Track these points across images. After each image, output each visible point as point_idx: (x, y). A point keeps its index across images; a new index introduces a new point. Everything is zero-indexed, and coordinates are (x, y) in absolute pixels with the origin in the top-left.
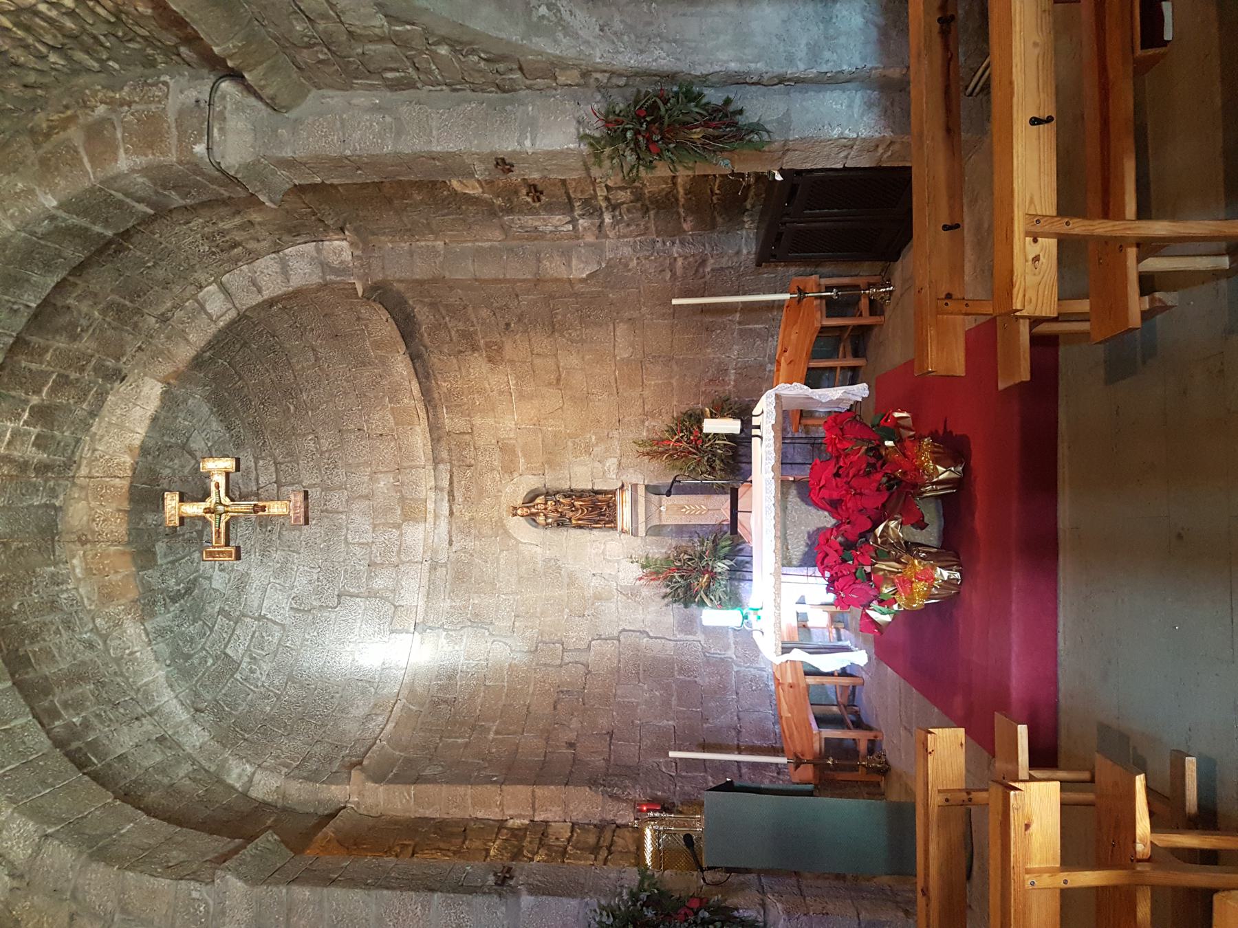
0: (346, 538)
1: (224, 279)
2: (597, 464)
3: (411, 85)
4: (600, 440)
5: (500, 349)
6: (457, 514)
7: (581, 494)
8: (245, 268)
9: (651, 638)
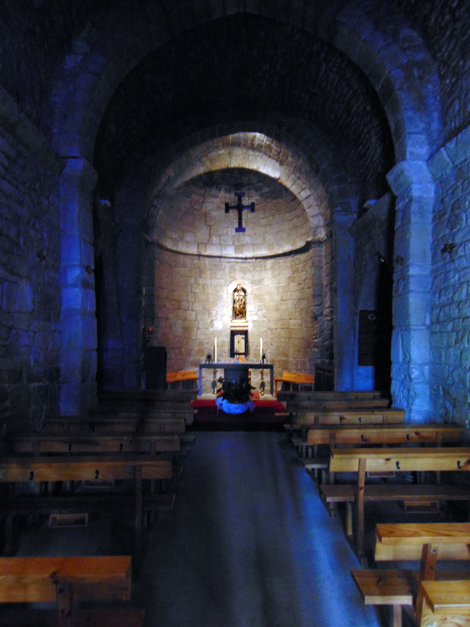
3: (355, 267)
6: (238, 265)
7: (244, 308)
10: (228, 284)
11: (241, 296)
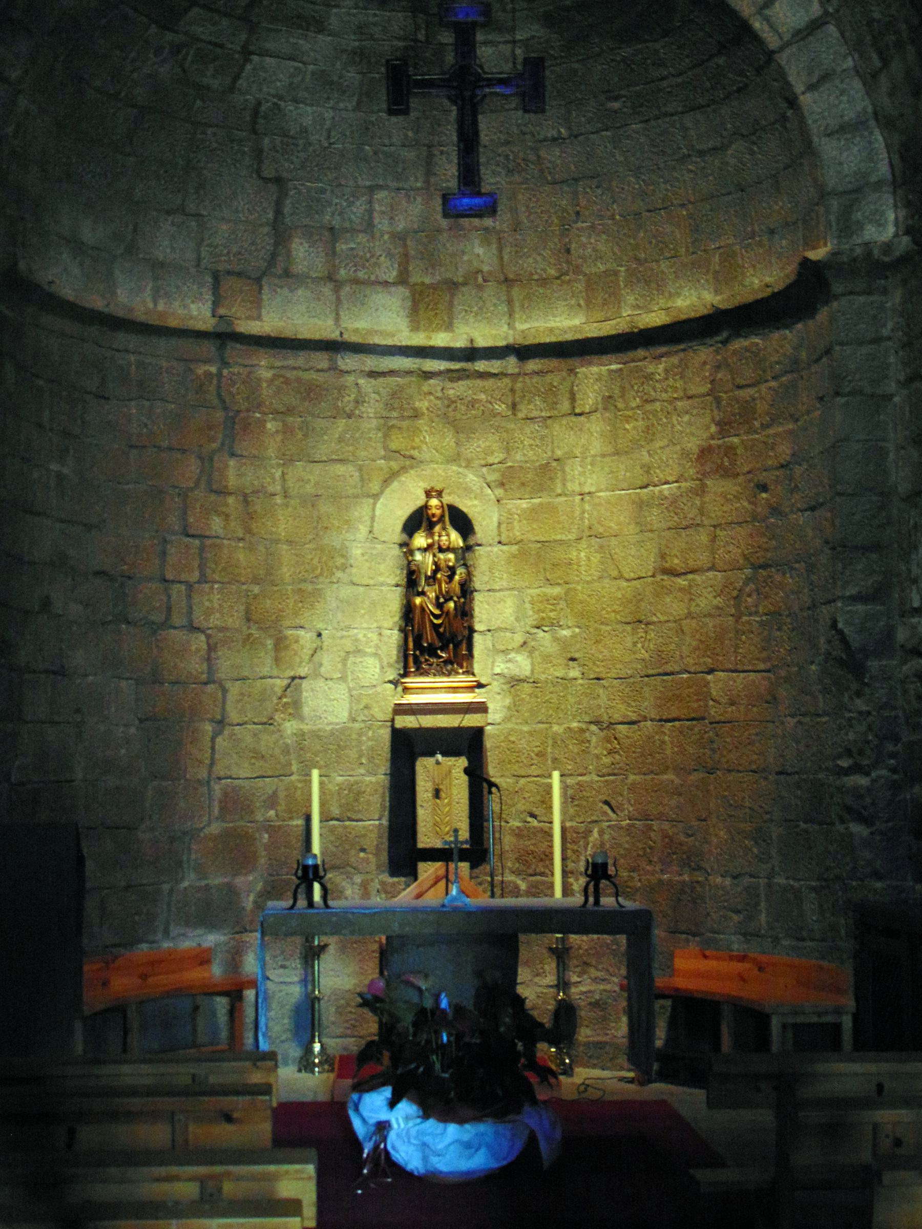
0: (380, 187)
1: (832, 29)
2: (519, 638)
4: (565, 645)
5: (727, 473)
7: (465, 612)
8: (849, 63)
9: (213, 740)
10: (375, 487)
11: (449, 549)
